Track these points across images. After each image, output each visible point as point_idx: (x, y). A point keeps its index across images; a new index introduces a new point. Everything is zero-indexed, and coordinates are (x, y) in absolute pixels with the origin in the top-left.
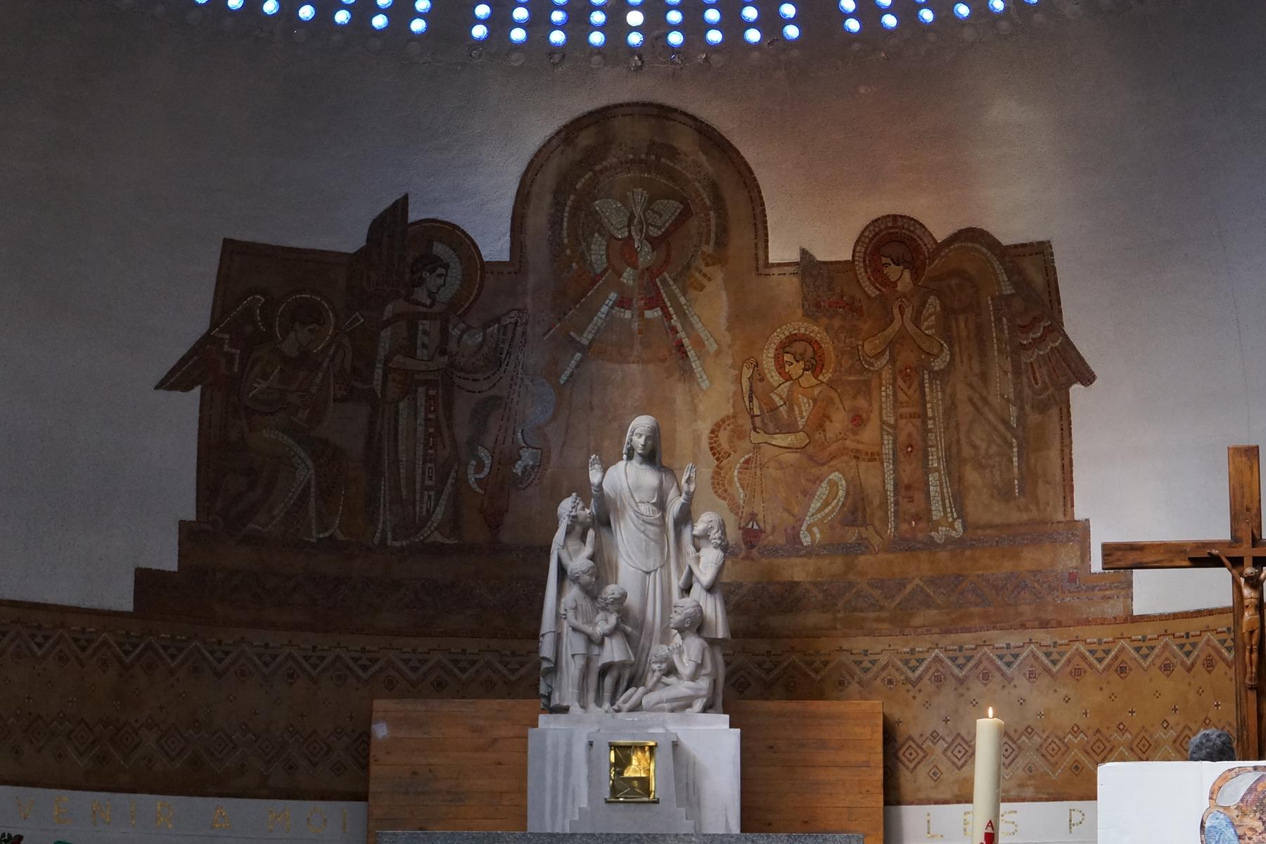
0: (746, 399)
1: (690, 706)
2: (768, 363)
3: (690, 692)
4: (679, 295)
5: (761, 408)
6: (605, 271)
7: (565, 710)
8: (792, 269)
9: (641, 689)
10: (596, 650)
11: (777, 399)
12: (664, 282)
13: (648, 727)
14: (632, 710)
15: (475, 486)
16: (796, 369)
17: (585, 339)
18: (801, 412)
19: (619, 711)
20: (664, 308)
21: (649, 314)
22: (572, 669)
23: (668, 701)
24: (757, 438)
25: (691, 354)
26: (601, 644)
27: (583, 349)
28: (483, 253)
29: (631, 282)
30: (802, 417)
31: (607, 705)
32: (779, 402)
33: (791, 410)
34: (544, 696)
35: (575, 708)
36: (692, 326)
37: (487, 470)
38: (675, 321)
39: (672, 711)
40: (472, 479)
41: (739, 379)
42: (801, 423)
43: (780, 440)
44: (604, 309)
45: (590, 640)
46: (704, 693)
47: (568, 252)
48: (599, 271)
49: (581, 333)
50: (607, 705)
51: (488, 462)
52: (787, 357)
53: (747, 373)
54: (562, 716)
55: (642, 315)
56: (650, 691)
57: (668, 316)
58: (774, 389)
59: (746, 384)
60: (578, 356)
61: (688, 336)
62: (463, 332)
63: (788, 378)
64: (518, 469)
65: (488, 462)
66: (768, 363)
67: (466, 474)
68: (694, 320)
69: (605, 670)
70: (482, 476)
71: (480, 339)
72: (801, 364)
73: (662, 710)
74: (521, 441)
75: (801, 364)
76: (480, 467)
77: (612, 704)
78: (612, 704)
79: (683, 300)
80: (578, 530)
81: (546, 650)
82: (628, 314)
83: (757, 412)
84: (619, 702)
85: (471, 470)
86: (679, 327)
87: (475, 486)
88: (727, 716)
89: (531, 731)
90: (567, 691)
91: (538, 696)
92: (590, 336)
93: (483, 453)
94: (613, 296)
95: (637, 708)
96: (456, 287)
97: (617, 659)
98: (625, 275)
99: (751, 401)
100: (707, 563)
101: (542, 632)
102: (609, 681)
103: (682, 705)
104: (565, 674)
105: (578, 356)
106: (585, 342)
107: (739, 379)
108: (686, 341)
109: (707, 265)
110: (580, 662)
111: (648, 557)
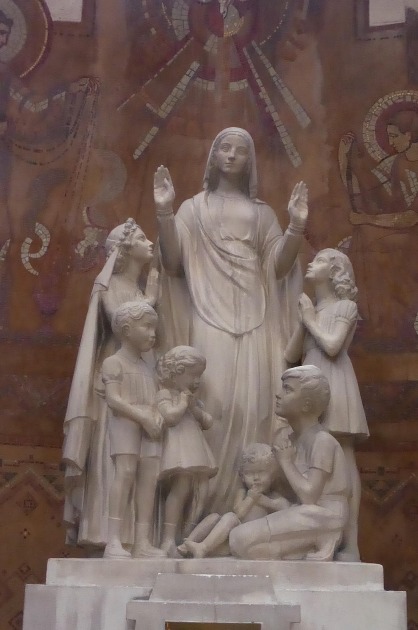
0: (345, 181)
1: (315, 548)
2: (369, 136)
3: (312, 524)
4: (268, 65)
5: (360, 186)
6: (187, 38)
7: (98, 551)
8: (395, 32)
9: (228, 518)
10: (153, 449)
11: (379, 175)
12: (252, 51)
13: (242, 592)
14: (210, 554)
15: (28, 266)
16: (402, 141)
17: (164, 111)
18: (409, 188)
19: (189, 555)
20: (252, 81)
21: (235, 86)
22: (111, 481)
23: (274, 538)
24: (356, 218)
25: (281, 129)
26: (162, 438)
27: (161, 123)
28: (52, 11)
29: (215, 51)
30: (411, 194)
31: (169, 542)
32: (382, 178)
33: (396, 187)
34: (69, 525)
35: (116, 549)
36: (281, 98)
37: (43, 251)
38: (263, 94)
39: (282, 556)
40: (25, 257)
41: (335, 155)
42: (409, 200)
43: (386, 220)
44: (185, 80)
45: (143, 432)
46: (337, 524)
47: (147, 15)
48: (180, 38)
49: (159, 102)
50: (169, 542)
51: (46, 241)
52: (391, 129)
53: (344, 149)
54: (89, 564)
55: (226, 87)
56: (242, 520)
57: (256, 89)
58: (375, 164)
59: (343, 161)
60: (155, 130)
61: (277, 110)
62: (25, 98)
63: (392, 151)
64: (81, 250)
65: (46, 241)
66: (369, 136)
67: (19, 253)
68: (285, 93)
69: (166, 485)
70: (37, 255)
71: (45, 107)
72: (408, 136)
73: (268, 556)
74: (85, 218)
75: (408, 136)
76: (36, 245)
77: (179, 542)
78: (179, 542)
79: (272, 72)
80: (134, 267)
81: (73, 450)
82: (211, 86)
83: (356, 190)
84: (190, 542)
85: (25, 249)
86: (268, 101)
87: (28, 266)
88: (379, 568)
89: (31, 589)
90: (101, 524)
91: (61, 524)
92: (169, 109)
93: (41, 231)
94: (195, 65)
95: (222, 549)
96: (20, 47)
97: (185, 465)
98: (209, 43)
99: (349, 177)
100: (332, 322)
101: (68, 418)
102: (174, 504)
103: (303, 547)
104: (100, 488)
105: (155, 130)
106: (163, 114)
107: (335, 155)
108: (275, 116)
109: (300, 32)
110: (126, 468)
111: (237, 315)
